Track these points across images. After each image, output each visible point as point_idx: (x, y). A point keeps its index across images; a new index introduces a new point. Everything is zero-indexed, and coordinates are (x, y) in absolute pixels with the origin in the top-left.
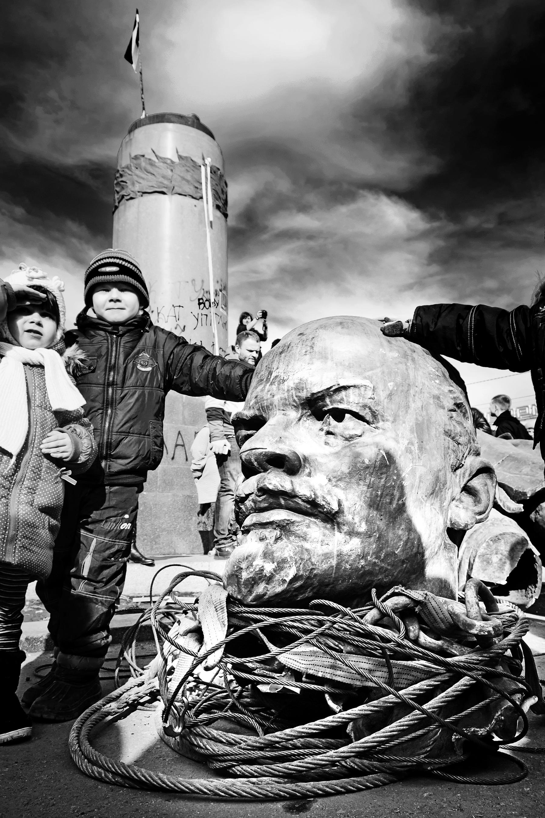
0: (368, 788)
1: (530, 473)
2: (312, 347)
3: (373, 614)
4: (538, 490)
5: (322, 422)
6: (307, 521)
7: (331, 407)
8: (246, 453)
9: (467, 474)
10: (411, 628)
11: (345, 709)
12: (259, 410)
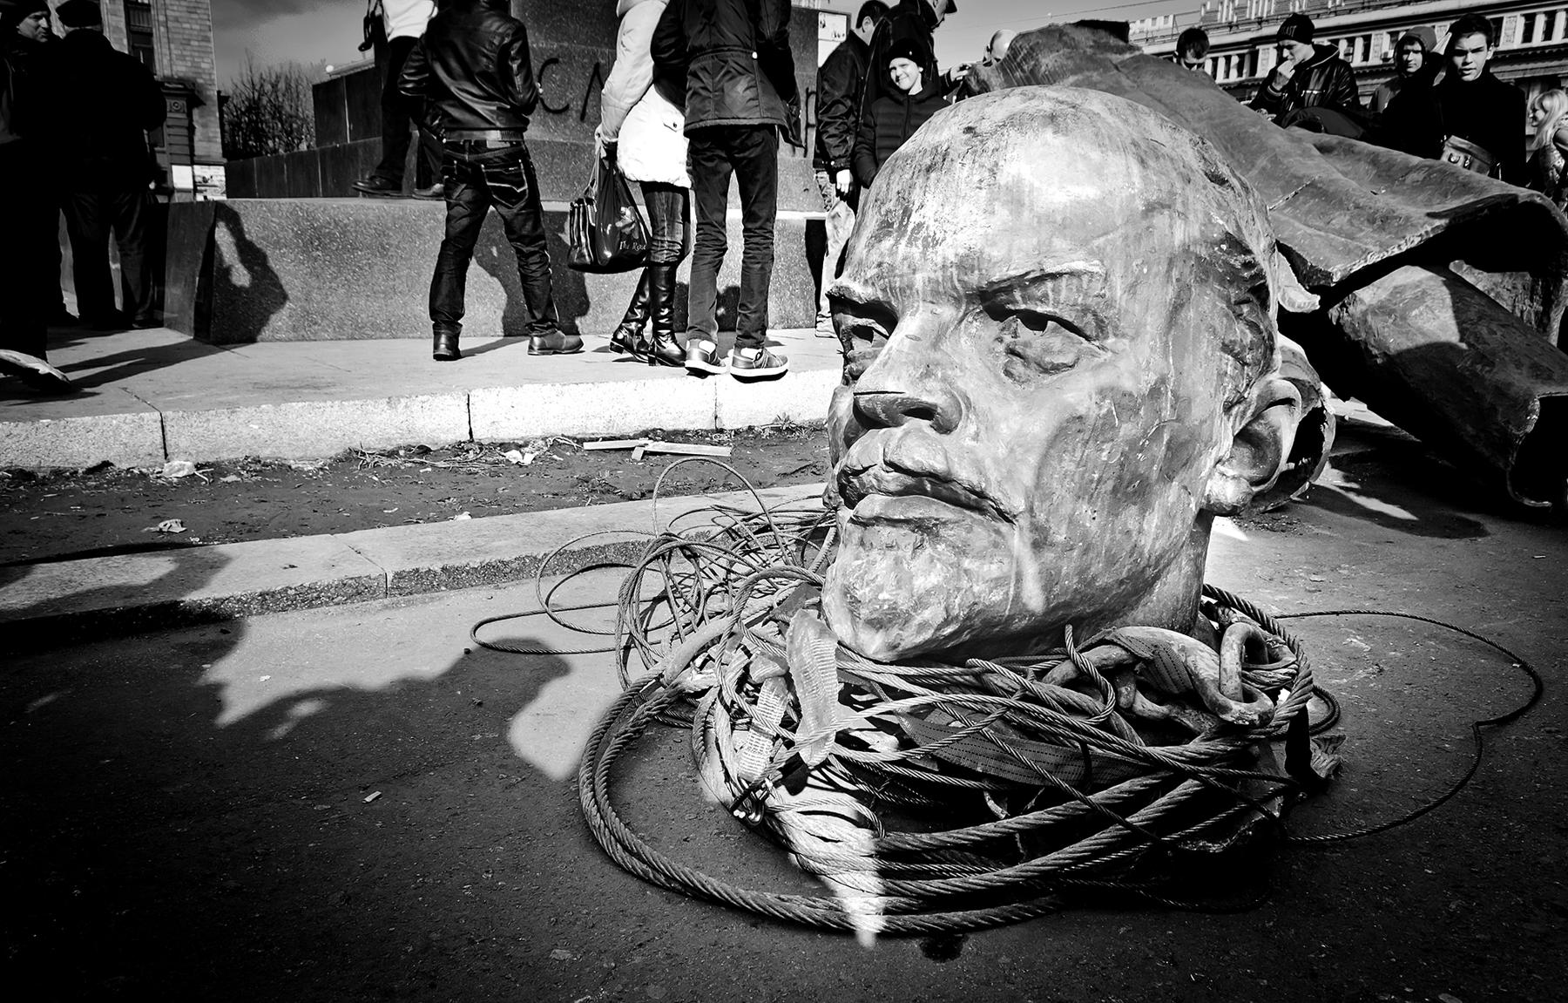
0: (1037, 916)
1: (1347, 227)
2: (993, 173)
3: (1065, 669)
4: (1356, 269)
5: (1001, 325)
6: (969, 521)
7: (1023, 307)
8: (867, 397)
9: (1249, 413)
10: (1123, 690)
11: (1013, 813)
12: (884, 290)
